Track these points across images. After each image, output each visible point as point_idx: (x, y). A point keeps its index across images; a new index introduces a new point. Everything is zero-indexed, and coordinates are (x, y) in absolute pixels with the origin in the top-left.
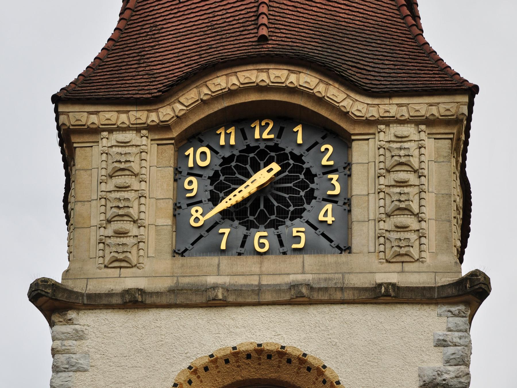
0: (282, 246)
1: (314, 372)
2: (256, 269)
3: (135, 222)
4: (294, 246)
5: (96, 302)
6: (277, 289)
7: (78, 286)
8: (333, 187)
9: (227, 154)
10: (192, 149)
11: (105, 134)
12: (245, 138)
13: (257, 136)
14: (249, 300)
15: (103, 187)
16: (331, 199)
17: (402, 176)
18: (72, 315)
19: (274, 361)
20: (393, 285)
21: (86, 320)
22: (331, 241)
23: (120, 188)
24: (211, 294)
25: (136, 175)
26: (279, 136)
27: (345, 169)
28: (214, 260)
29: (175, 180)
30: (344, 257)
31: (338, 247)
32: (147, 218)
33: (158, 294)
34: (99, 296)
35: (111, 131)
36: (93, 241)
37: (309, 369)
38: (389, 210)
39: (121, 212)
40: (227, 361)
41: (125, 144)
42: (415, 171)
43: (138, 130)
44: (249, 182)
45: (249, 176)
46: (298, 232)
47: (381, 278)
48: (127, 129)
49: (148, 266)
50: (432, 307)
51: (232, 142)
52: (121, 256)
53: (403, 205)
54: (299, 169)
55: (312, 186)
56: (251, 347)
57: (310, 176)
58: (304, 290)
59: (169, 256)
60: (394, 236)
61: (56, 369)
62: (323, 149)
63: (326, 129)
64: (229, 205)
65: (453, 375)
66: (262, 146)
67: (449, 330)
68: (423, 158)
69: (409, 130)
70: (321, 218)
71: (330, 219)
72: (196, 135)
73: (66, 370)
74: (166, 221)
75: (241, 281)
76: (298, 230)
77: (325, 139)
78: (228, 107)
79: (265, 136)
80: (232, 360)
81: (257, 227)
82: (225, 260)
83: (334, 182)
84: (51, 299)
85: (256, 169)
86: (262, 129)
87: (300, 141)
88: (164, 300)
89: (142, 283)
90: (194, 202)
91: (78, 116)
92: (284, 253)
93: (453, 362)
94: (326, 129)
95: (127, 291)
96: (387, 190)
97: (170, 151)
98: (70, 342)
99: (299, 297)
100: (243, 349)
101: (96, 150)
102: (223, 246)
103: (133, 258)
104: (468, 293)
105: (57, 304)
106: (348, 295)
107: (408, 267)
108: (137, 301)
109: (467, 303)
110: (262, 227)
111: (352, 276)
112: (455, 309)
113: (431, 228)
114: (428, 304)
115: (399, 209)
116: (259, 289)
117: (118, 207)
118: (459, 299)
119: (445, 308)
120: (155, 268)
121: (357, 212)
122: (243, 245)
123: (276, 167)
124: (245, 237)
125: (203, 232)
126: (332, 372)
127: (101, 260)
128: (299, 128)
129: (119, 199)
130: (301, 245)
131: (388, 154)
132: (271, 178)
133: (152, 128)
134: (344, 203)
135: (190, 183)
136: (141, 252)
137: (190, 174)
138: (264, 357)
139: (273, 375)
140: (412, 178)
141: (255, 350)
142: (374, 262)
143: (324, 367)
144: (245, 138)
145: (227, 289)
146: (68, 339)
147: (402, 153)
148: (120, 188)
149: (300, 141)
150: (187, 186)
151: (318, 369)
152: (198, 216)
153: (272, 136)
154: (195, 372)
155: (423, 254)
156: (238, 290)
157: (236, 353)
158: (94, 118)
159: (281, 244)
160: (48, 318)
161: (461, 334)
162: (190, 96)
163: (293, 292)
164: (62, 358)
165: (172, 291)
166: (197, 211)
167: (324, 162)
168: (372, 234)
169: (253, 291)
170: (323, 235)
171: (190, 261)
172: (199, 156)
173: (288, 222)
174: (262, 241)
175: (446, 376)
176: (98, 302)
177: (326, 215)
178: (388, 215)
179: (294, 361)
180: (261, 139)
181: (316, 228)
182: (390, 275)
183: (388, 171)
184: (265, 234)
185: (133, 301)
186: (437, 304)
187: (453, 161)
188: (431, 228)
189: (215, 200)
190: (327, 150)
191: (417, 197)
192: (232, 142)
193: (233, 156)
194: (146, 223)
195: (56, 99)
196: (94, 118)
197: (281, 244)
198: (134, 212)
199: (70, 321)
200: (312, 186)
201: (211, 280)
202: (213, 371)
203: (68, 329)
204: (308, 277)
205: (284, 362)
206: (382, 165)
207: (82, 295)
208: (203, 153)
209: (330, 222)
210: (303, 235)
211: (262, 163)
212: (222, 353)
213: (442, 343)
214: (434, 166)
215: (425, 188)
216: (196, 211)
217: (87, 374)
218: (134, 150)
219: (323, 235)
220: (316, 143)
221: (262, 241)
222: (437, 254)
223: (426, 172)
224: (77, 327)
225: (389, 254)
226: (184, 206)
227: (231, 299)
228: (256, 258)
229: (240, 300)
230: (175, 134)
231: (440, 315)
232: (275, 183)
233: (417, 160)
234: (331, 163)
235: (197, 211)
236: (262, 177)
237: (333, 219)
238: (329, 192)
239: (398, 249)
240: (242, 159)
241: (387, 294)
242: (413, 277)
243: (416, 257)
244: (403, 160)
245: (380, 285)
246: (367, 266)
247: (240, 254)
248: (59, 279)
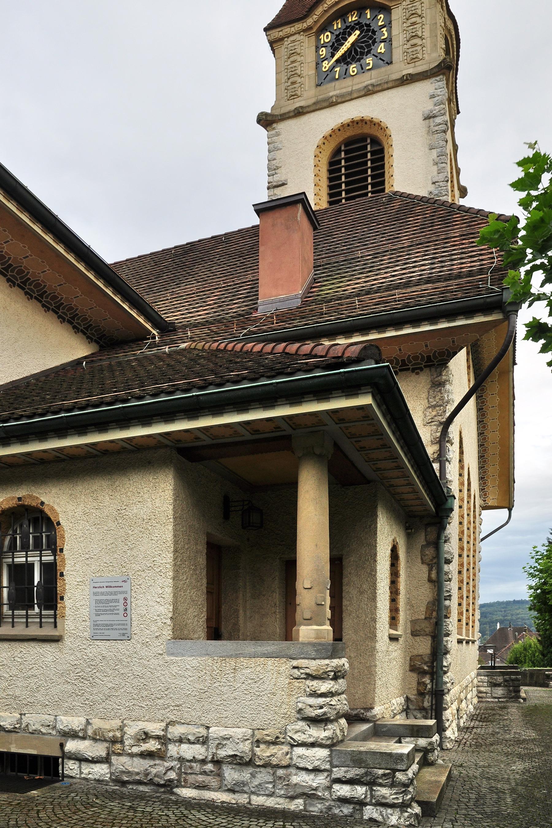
1: (377, 125)
2: (350, 83)
3: (299, 76)
4: (368, 68)
5: (284, 117)
6: (359, 90)
7: (277, 112)
8: (384, 35)
9: (338, 33)
11: (286, 39)
12: (345, 23)
13: (350, 20)
14: (347, 99)
15: (286, 64)
16: (384, 41)
17: (413, 20)
18: (274, 125)
19: (360, 125)
20: (409, 74)
21: (281, 127)
22: (383, 61)
23: (293, 62)
24: (331, 100)
25: (299, 54)
26: (360, 18)
27: (388, 24)
28: (333, 84)
29: (316, 52)
30: (389, 67)
31: (387, 63)
32: (304, 73)
33: (308, 106)
34: (285, 114)
35: (288, 37)
36: (283, 89)
37: (375, 124)
38: (408, 38)
39: (293, 73)
40: (339, 130)
41: (294, 41)
42: (420, 16)
43: (299, 33)
44: (346, 43)
45: (346, 40)
47: (405, 72)
48: (295, 34)
49: (306, 95)
50: (428, 80)
52: (293, 94)
53: (414, 34)
54: (363, 26)
55: (375, 37)
56: (349, 121)
57: (374, 32)
58: (370, 88)
59: (314, 88)
60: (411, 50)
61: (269, 151)
62: (379, 18)
63: (380, 7)
64: (338, 56)
65: (437, 110)
66: (353, 24)
67: (436, 89)
68: (423, 8)
70: (379, 51)
71: (383, 51)
72: (323, 29)
73: (273, 151)
74: (312, 72)
75: (344, 90)
76: (369, 60)
77: (380, 12)
78: (336, 10)
79: (354, 19)
80: (341, 129)
81: (351, 64)
82: (337, 83)
84: (266, 121)
85: (350, 35)
86: (352, 16)
87: (369, 17)
88: (312, 109)
89: (302, 104)
90: (325, 59)
91: (274, 34)
92: (364, 72)
93: (437, 104)
94: (380, 7)
95: (296, 109)
96: (407, 29)
97: (313, 38)
98: (274, 138)
99: (369, 91)
100: (345, 122)
101: (283, 47)
102: (337, 77)
103: (299, 93)
104: (444, 68)
105: (268, 122)
106: (390, 85)
107: (417, 64)
108: (300, 112)
109: (443, 74)
110: (353, 63)
111: (392, 75)
112: (438, 78)
113: (428, 42)
114: (426, 79)
115: (413, 36)
116: (351, 93)
117: (292, 71)
118: (440, 73)
119: (434, 79)
120: (308, 94)
121: (395, 44)
122: (345, 74)
123: (358, 32)
124: (346, 69)
125: (328, 72)
126: (384, 123)
127: (286, 98)
128: (368, 11)
129: (292, 68)
130: (370, 67)
131: (407, 11)
132: (356, 39)
133: (304, 31)
134: (389, 41)
135: (322, 51)
136: (302, 89)
137: (322, 47)
138: (355, 124)
139: (360, 132)
140: (418, 20)
141: (351, 122)
142: (402, 66)
143: (381, 122)
144: (345, 23)
145: (337, 96)
146: (273, 137)
147: (413, 9)
148: (293, 62)
149: (369, 17)
150: (321, 53)
151: (378, 123)
152: (326, 65)
153: (357, 18)
154: (326, 138)
155: (424, 56)
156: (342, 96)
157: (343, 125)
158: (281, 34)
159: (362, 69)
160: (266, 129)
161: (441, 90)
162: (319, 10)
163: (365, 90)
164: (271, 146)
165: (314, 104)
167: (380, 24)
168: (401, 52)
169: (348, 94)
170: (380, 59)
171: (323, 87)
172: (326, 38)
173: (365, 57)
174: (354, 69)
175: (434, 112)
176: (285, 117)
177: (381, 49)
178: (408, 41)
179: (368, 122)
180: (352, 21)
181: (377, 57)
182: (411, 70)
183: (408, 19)
185: (299, 113)
186: (430, 78)
187: (439, 6)
188: (428, 42)
189: (333, 56)
191: (421, 28)
192: (339, 26)
193: (340, 33)
194: (304, 75)
195: (266, 30)
196: (281, 34)
197: (362, 69)
198: (298, 72)
199: (274, 129)
200: (375, 37)
201: (331, 94)
202: (334, 136)
203: (273, 132)
204: (373, 81)
205: (364, 124)
206: (405, 17)
207: (278, 115)
208: (328, 35)
209: (383, 52)
210: (371, 62)
212: (337, 127)
213: (432, 97)
214: (428, 11)
215: (424, 23)
216: (325, 64)
217: (282, 150)
218: (298, 43)
219: (380, 59)
220: (376, 16)
221: (354, 69)
222: (430, 54)
223: (424, 15)
224: (277, 130)
225: (409, 59)
226: (320, 62)
227: (339, 100)
228: (351, 78)
229: (343, 100)
230: (314, 30)
231: (432, 83)
232: (359, 40)
233: (420, 10)
234: (383, 23)
236: (352, 39)
238: (383, 38)
239: (412, 56)
240: (344, 33)
241: (407, 80)
242: (421, 67)
243: (421, 58)
244: (414, 12)
245: (403, 76)
246: (401, 68)
248: (269, 111)
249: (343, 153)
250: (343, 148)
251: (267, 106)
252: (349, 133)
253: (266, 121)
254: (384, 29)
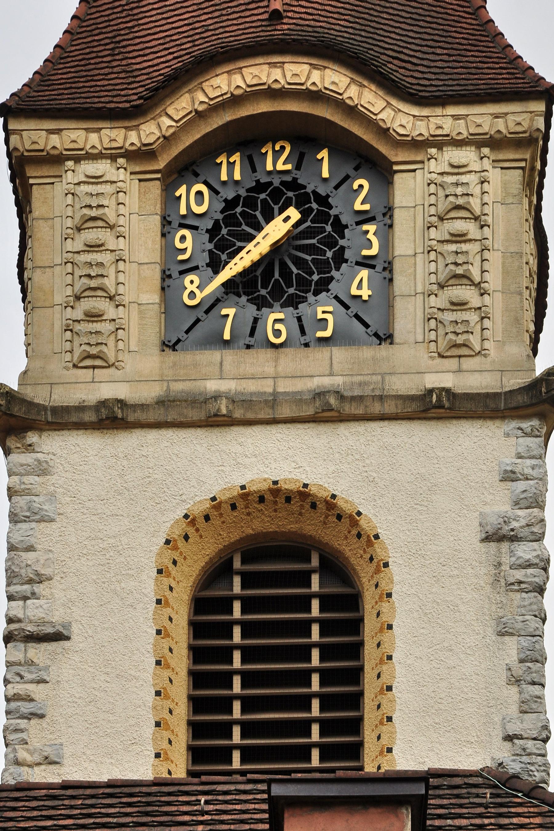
0: (304, 335)
4: (320, 334)
8: (369, 244)
10: (184, 187)
16: (366, 263)
46: (324, 312)
51: (237, 176)
62: (355, 186)
69: (467, 156)
70: (354, 291)
71: (365, 293)
76: (324, 309)
83: (370, 236)
166: (192, 282)
167: (358, 206)
177: (360, 287)
184: (281, 316)
190: (361, 186)
208: (199, 193)
211: (276, 208)
234: (367, 207)
235: (192, 282)
237: (370, 293)
238: (365, 252)
247: (248, 347)
249: (237, 581)
250: (237, 564)
254: (371, 228)
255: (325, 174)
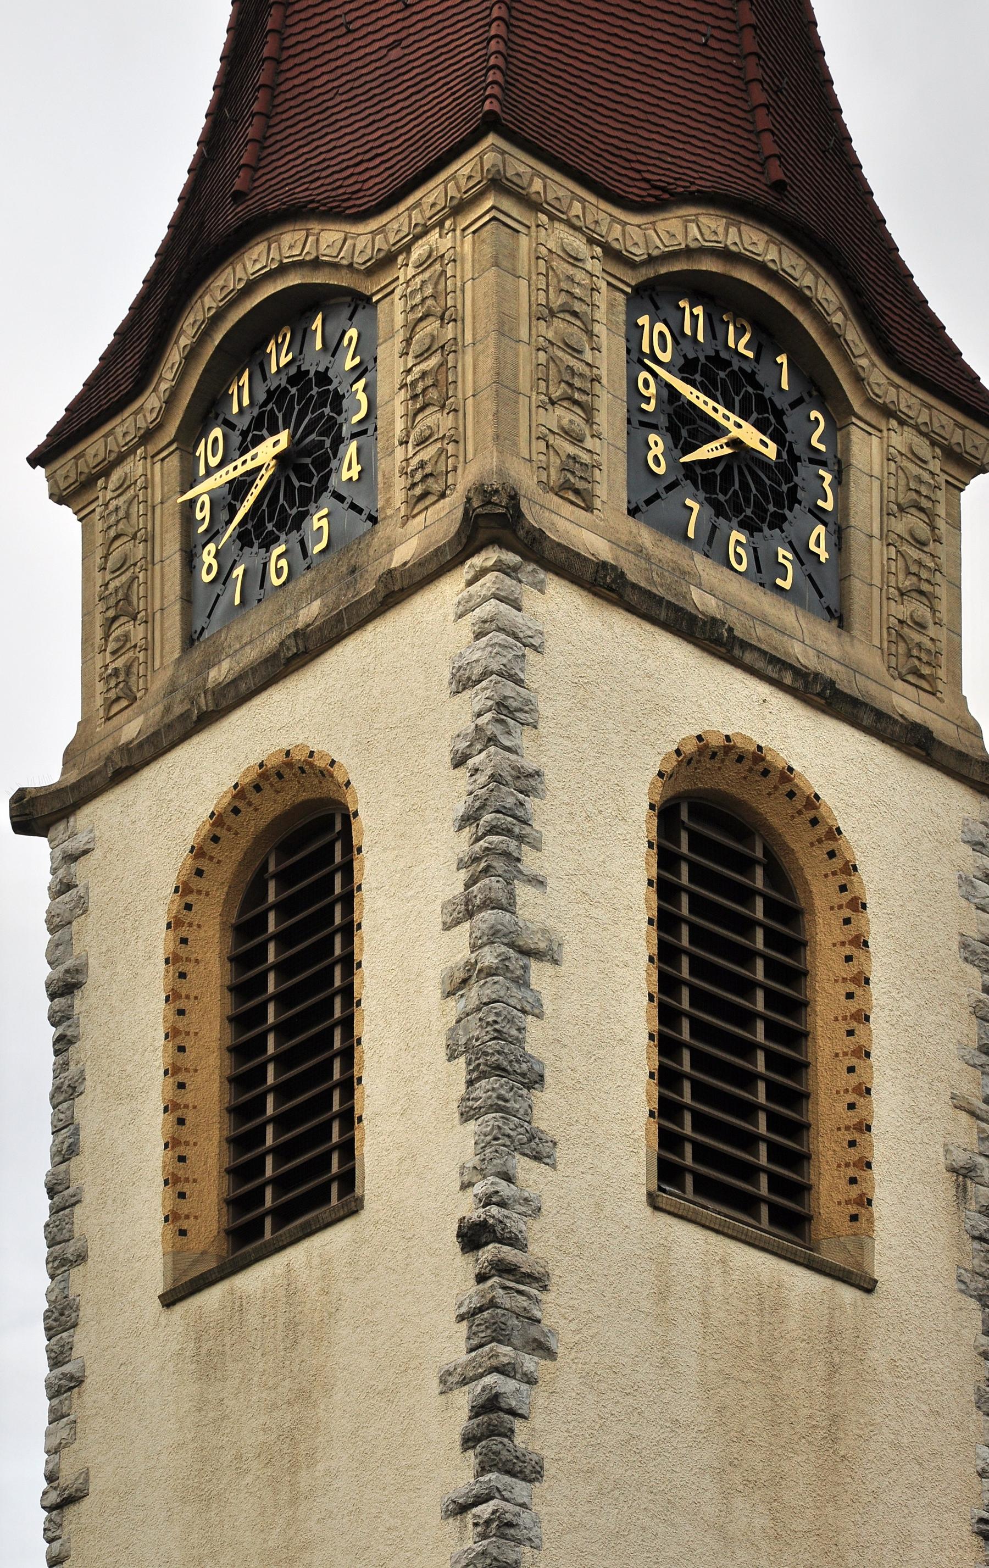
35: (106, 472)
46: (319, 519)
251: (47, 772)
252: (272, 806)
253: (32, 814)
255: (319, 345)
